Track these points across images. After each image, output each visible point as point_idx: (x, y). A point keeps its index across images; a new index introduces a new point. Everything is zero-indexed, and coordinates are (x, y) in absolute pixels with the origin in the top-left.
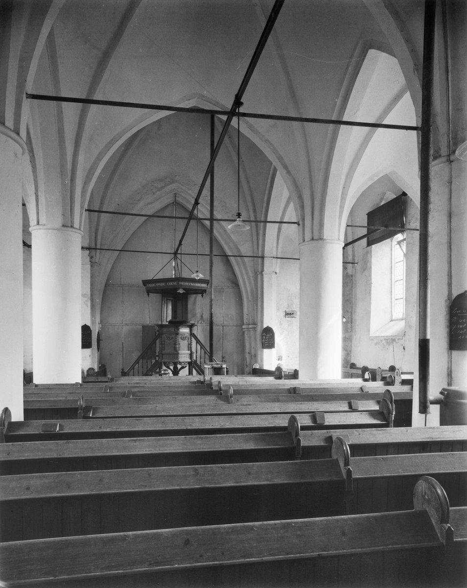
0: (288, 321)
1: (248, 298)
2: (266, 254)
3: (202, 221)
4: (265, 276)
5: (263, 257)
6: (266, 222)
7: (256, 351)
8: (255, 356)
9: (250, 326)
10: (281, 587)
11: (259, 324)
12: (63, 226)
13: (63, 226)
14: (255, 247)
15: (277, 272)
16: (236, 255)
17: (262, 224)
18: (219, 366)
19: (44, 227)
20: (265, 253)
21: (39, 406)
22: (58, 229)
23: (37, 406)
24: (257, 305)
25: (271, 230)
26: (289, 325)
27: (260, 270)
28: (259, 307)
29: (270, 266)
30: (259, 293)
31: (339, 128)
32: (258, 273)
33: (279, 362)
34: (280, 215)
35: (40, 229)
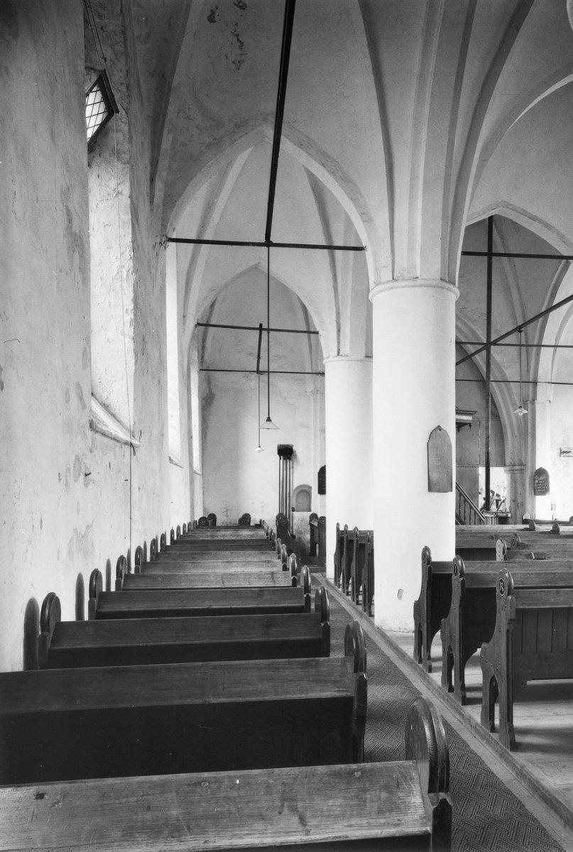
0: (564, 461)
1: (512, 433)
2: (540, 379)
3: (463, 345)
4: (537, 405)
5: (535, 383)
6: (540, 346)
7: (524, 498)
8: (523, 504)
9: (517, 467)
10: (305, 851)
11: (529, 465)
12: (366, 356)
13: (366, 356)
14: (524, 369)
15: (551, 400)
16: (500, 380)
17: (535, 348)
18: (505, 514)
19: (347, 359)
20: (539, 377)
21: (212, 536)
22: (361, 361)
23: (466, 546)
24: (526, 442)
25: (546, 354)
26: (564, 466)
27: (530, 398)
28: (530, 441)
29: (544, 392)
30: (530, 426)
31: (200, 248)
32: (529, 402)
33: (553, 512)
34: (209, 338)
35: (343, 360)
